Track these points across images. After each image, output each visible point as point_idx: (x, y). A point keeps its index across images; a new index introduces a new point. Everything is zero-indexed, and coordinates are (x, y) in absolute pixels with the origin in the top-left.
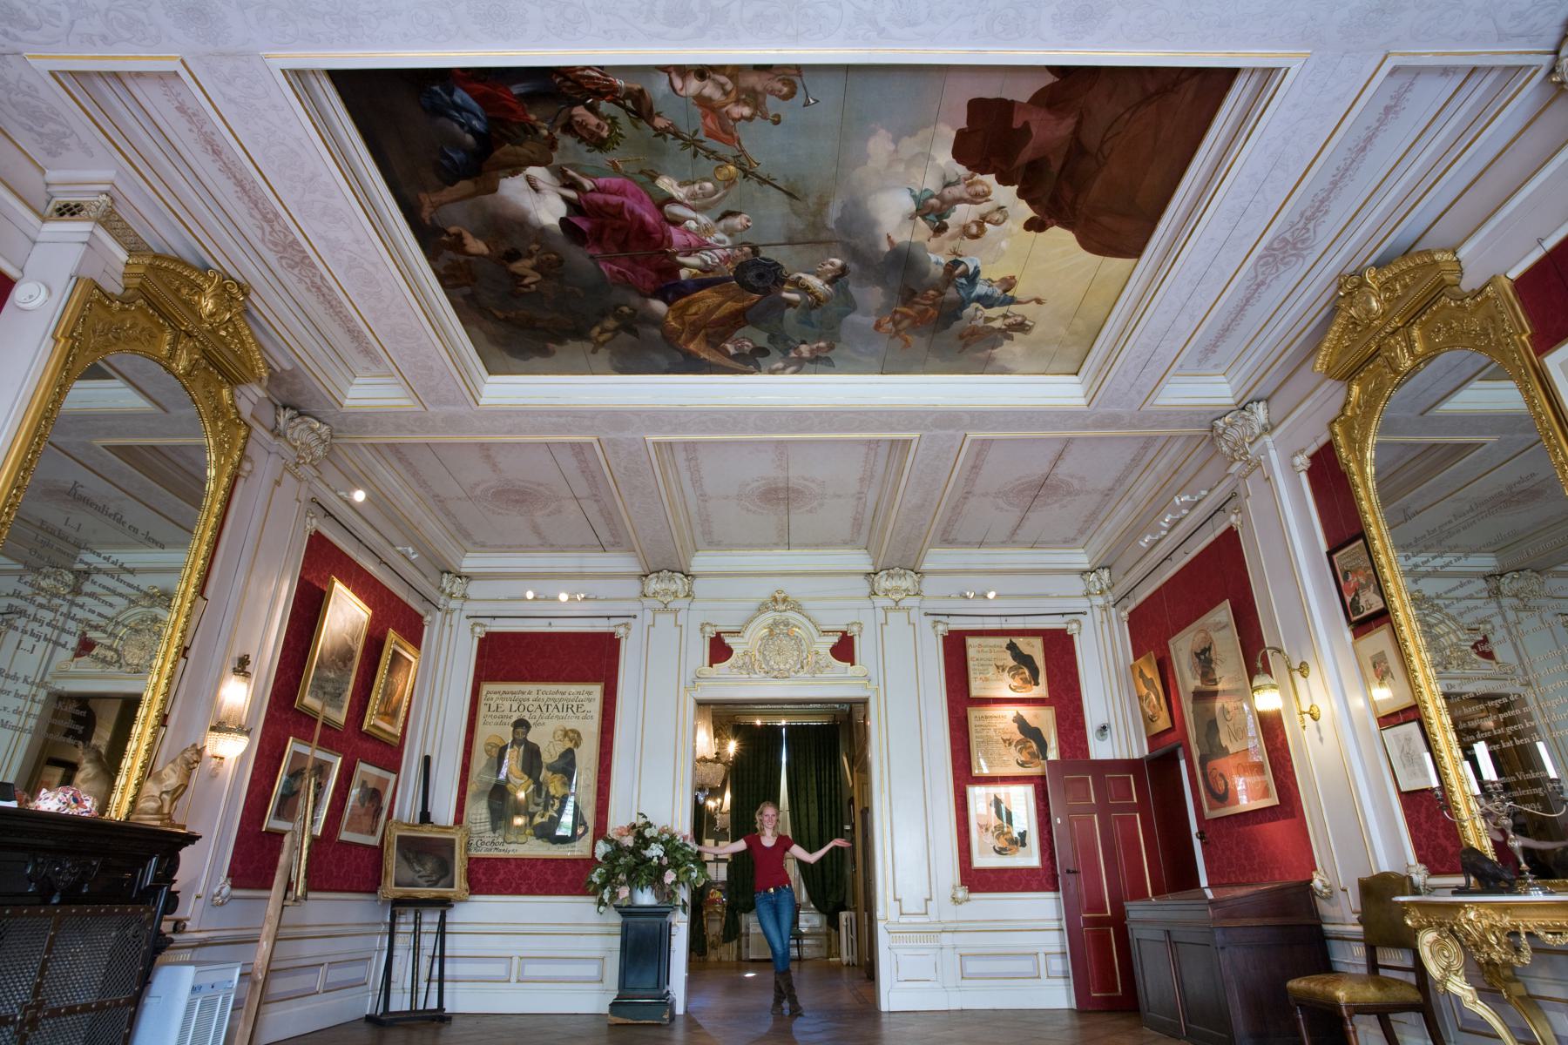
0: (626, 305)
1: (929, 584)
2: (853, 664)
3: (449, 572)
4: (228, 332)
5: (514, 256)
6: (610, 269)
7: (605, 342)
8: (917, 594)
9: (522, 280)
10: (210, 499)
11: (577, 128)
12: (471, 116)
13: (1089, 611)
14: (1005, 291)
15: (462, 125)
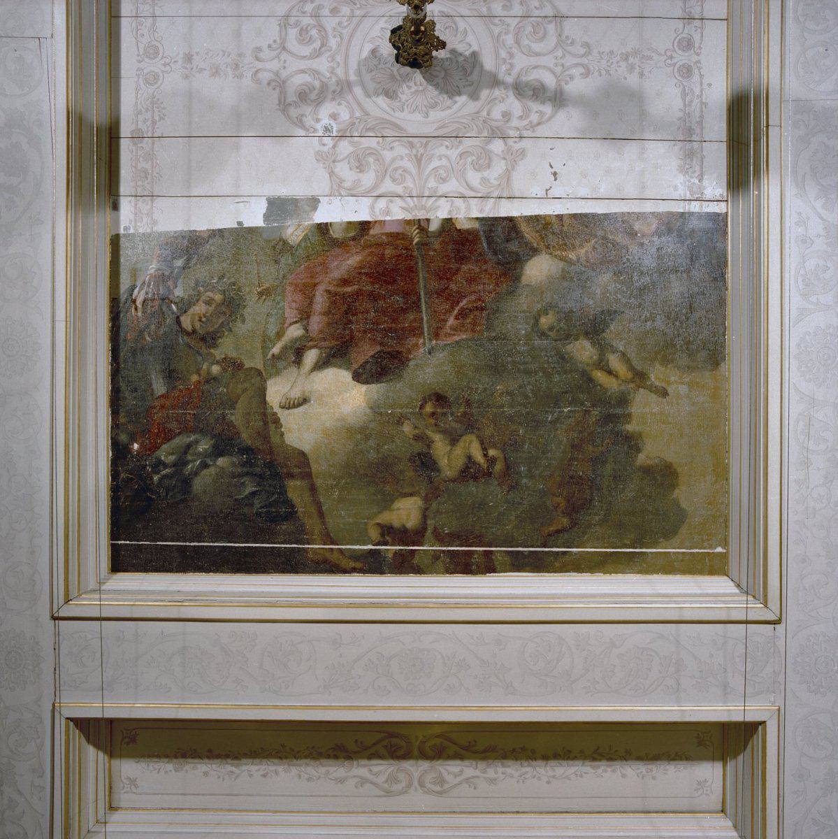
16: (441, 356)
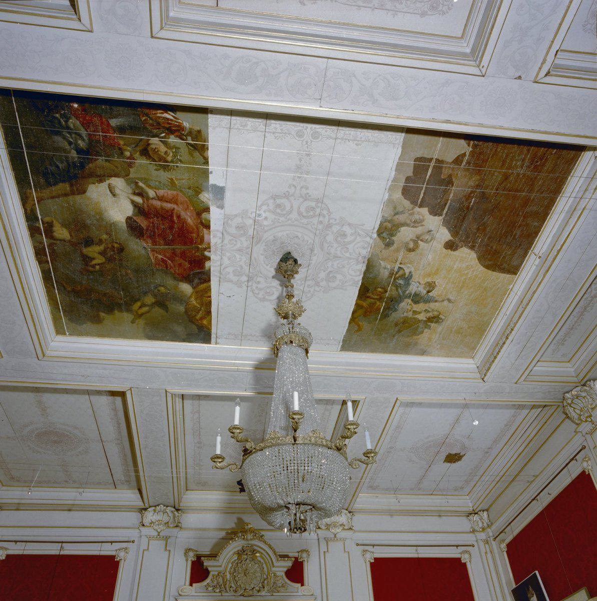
0: (162, 286)
1: (359, 521)
2: (302, 585)
5: (89, 242)
6: (156, 257)
7: (142, 314)
9: (91, 261)
11: (151, 153)
12: (78, 137)
13: (475, 544)
14: (428, 292)
15: (70, 143)
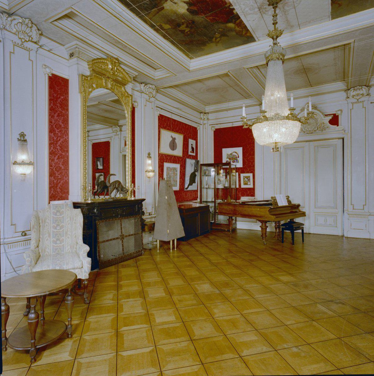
0: (220, 28)
2: (338, 125)
3: (202, 113)
4: (117, 72)
8: (368, 95)
9: (185, 32)
10: (127, 119)
16: (203, 19)
